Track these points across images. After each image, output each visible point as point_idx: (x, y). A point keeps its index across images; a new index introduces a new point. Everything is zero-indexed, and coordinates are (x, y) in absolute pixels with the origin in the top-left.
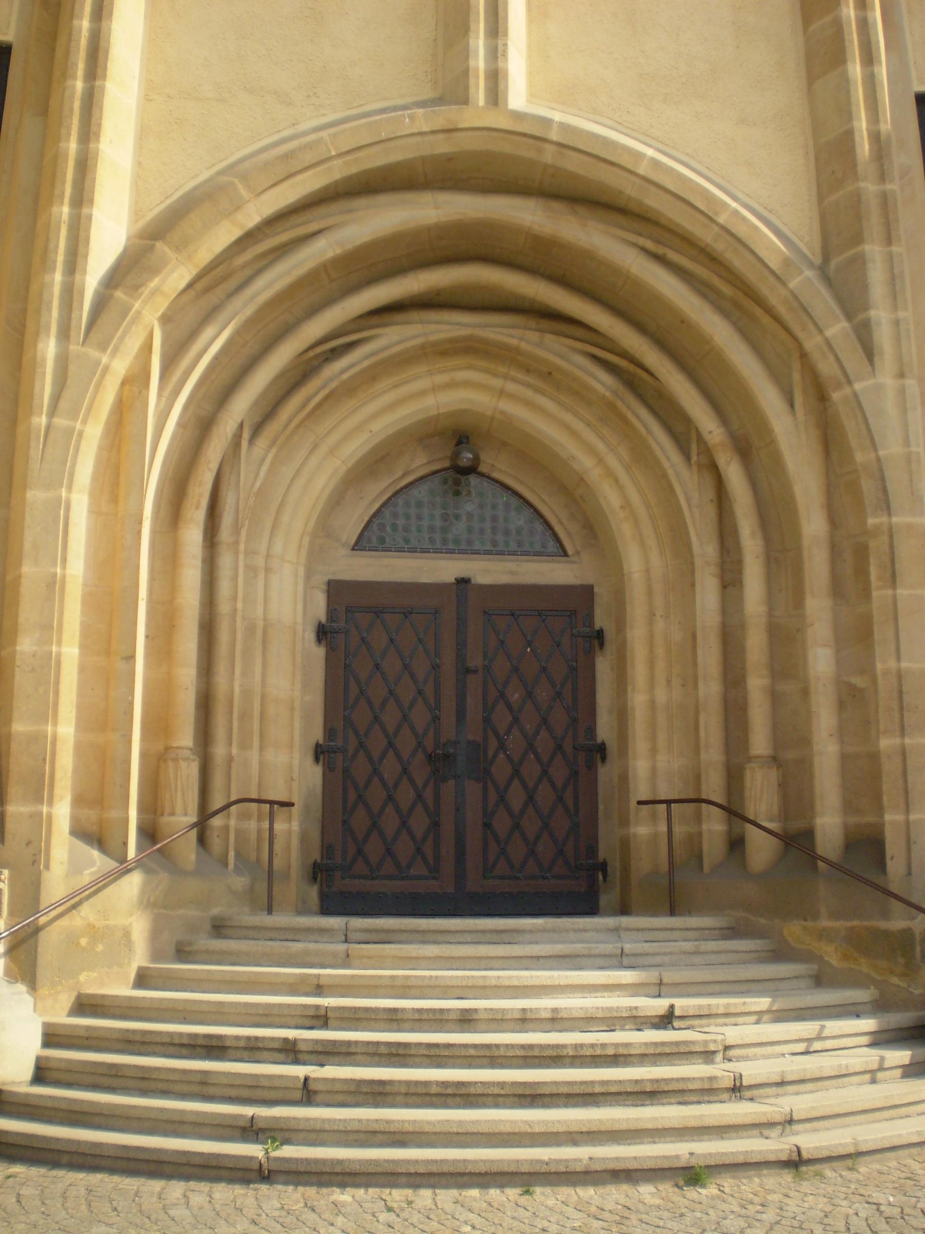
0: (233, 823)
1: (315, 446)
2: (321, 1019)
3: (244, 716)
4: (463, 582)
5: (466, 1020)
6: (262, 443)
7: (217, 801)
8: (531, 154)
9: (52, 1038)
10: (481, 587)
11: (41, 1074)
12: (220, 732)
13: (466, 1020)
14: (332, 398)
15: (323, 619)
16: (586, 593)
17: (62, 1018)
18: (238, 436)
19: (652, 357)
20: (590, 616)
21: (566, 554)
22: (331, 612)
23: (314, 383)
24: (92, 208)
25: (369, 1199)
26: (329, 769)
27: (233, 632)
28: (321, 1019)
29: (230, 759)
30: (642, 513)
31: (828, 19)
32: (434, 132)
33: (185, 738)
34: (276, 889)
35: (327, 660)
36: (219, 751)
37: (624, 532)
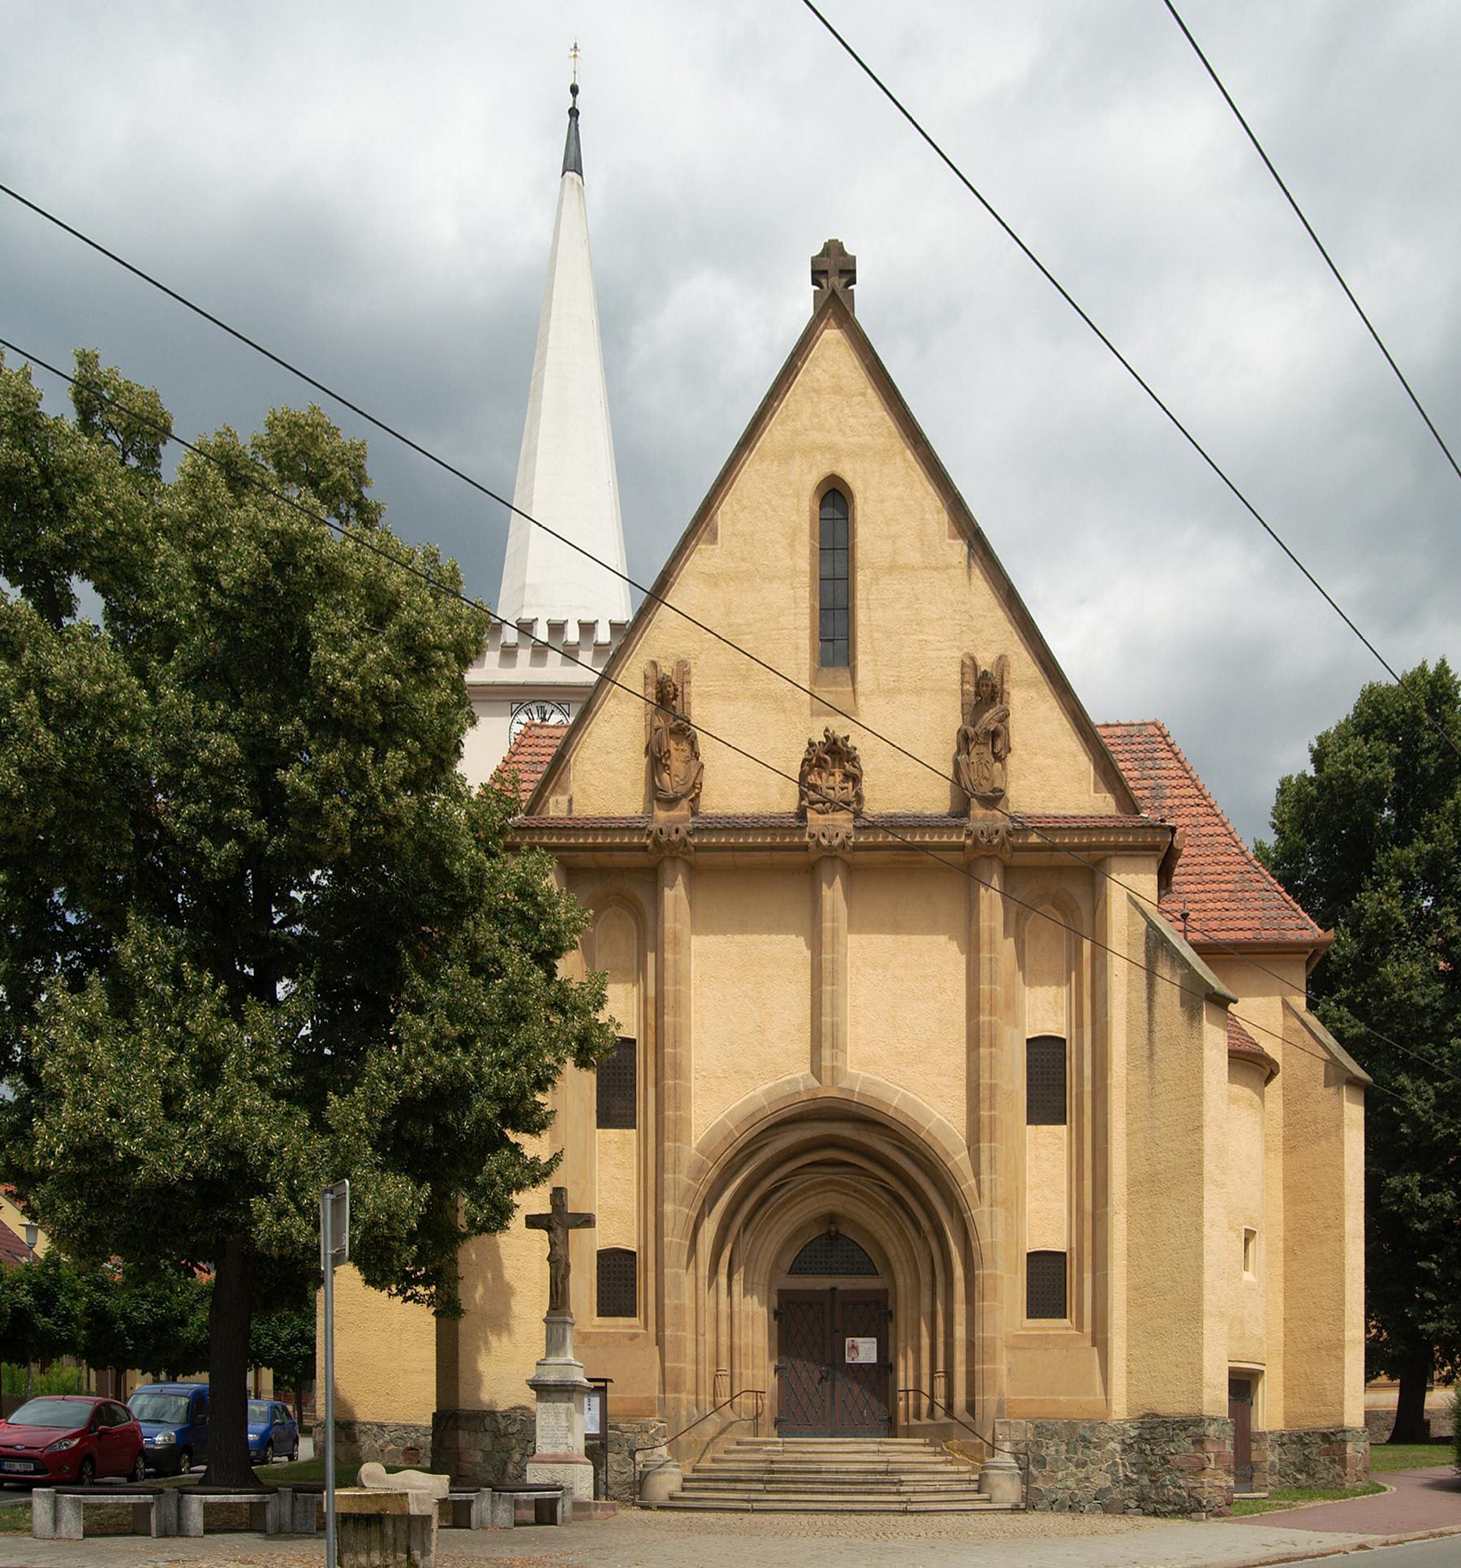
0: (743, 1400)
1: (770, 1231)
2: (772, 1472)
3: (745, 1354)
4: (833, 1289)
5: (818, 1472)
6: (748, 1233)
7: (736, 1392)
8: (846, 1107)
9: (685, 1480)
10: (841, 1291)
11: (684, 1489)
12: (736, 1363)
13: (818, 1472)
14: (778, 1209)
15: (776, 1308)
16: (885, 1292)
17: (689, 1474)
18: (738, 1234)
19: (902, 1191)
20: (886, 1305)
21: (877, 1274)
22: (780, 1305)
23: (768, 1204)
24: (546, 660)
25: (748, 1373)
26: (780, 1377)
27: (740, 1319)
28: (772, 1472)
29: (741, 1374)
30: (903, 1258)
31: (976, 1021)
32: (808, 1100)
33: (724, 1365)
34: (549, 238)
35: (779, 1326)
36: (737, 1371)
37: (896, 1266)
